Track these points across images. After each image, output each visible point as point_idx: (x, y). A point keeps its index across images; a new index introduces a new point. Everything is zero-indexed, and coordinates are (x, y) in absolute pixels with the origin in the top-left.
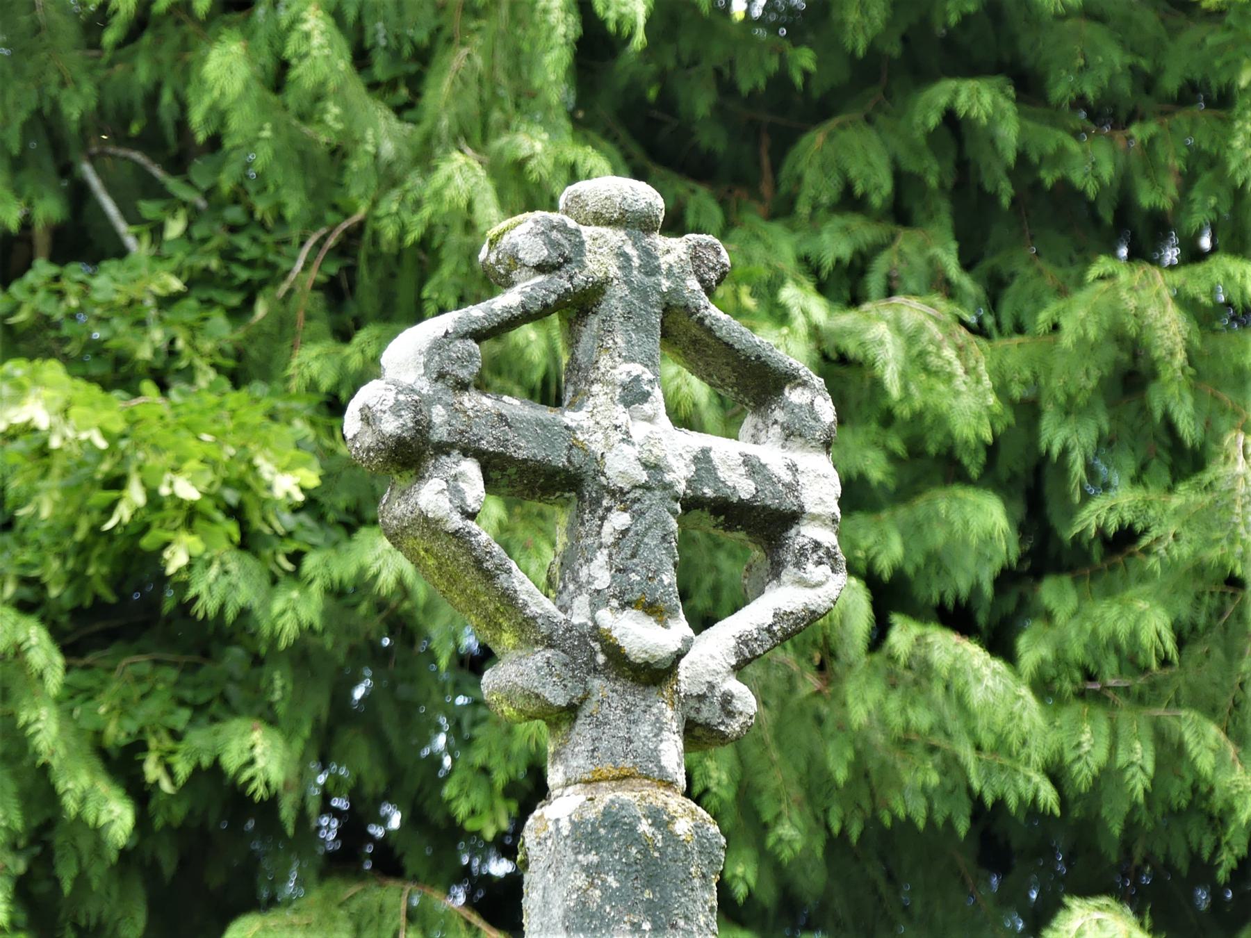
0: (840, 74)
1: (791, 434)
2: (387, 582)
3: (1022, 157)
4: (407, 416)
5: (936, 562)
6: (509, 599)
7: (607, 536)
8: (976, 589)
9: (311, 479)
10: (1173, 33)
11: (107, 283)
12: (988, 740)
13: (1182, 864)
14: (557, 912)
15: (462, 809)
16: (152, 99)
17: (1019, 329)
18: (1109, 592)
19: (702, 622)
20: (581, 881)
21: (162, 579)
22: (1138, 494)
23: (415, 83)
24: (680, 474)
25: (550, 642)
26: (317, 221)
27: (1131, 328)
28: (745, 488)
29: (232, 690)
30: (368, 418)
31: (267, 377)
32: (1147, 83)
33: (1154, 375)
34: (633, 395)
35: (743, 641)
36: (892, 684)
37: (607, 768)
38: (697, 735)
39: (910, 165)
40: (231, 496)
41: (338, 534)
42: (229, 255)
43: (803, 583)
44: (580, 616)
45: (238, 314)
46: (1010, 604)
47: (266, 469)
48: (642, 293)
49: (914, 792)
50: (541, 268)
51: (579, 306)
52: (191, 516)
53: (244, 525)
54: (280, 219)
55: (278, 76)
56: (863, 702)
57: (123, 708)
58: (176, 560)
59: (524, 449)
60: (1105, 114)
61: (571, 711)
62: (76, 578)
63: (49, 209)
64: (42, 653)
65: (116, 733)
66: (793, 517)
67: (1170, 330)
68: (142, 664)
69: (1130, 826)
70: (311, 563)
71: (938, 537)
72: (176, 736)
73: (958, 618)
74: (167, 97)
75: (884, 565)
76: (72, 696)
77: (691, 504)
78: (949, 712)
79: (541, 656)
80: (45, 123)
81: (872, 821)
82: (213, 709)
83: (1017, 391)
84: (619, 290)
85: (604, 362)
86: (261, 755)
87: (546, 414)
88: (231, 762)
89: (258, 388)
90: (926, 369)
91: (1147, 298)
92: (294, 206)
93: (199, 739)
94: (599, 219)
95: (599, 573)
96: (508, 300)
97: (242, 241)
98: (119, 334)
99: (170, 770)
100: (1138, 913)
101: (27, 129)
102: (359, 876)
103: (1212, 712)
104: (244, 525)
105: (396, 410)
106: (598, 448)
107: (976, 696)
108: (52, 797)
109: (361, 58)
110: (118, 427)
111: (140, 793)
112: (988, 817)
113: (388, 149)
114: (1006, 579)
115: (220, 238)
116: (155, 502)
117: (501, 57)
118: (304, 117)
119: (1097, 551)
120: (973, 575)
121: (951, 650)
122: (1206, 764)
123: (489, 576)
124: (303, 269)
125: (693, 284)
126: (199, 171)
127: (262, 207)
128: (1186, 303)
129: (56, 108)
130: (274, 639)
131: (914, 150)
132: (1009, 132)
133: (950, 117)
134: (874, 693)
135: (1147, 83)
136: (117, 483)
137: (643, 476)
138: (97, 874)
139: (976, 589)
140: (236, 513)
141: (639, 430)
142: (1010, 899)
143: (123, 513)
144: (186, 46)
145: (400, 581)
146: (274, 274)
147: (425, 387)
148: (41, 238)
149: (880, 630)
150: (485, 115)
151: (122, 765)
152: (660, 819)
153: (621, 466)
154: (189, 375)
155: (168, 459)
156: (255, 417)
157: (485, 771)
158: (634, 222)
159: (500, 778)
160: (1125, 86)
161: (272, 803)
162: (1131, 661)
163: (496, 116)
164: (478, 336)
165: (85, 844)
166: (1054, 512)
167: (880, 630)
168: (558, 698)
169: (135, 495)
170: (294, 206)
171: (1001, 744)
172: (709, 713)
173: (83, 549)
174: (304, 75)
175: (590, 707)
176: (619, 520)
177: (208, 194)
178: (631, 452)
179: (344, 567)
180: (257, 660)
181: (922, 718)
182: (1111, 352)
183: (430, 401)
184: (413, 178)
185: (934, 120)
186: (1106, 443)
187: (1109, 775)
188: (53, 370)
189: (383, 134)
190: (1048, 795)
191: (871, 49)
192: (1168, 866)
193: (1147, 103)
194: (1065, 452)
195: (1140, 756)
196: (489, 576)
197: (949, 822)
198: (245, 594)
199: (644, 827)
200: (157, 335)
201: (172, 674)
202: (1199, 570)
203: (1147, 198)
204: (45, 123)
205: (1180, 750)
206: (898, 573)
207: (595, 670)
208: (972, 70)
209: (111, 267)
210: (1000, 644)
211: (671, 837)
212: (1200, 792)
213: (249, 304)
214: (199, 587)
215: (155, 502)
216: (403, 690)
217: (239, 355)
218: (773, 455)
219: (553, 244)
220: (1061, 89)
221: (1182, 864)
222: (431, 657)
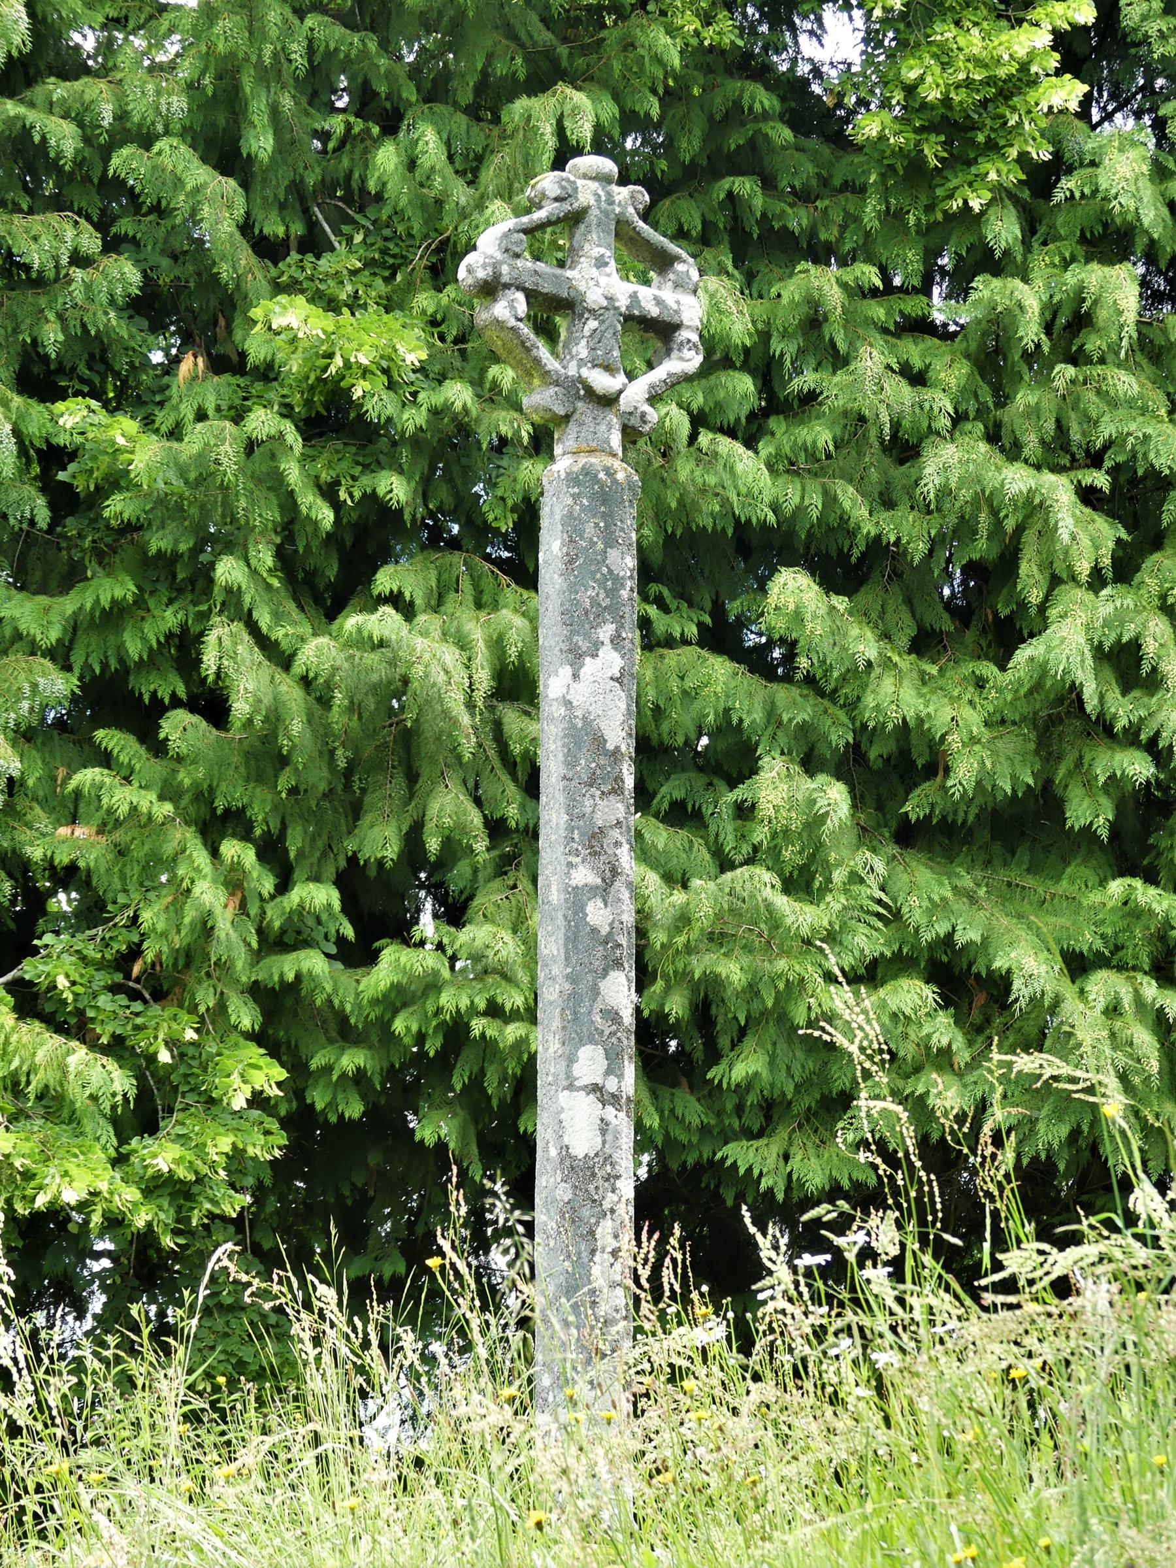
0: (679, 173)
1: (677, 286)
2: (458, 406)
3: (764, 215)
4: (490, 270)
5: (719, 406)
6: (537, 361)
7: (587, 332)
8: (738, 420)
9: (424, 356)
10: (838, 159)
11: (326, 263)
12: (744, 490)
13: (834, 554)
14: (558, 517)
15: (491, 517)
16: (349, 176)
17: (761, 297)
18: (802, 422)
19: (631, 376)
20: (570, 501)
21: (350, 401)
22: (818, 376)
23: (476, 171)
24: (623, 303)
25: (557, 383)
26: (426, 236)
27: (816, 295)
28: (654, 311)
29: (382, 458)
30: (470, 271)
31: (402, 309)
32: (825, 182)
33: (826, 319)
34: (600, 263)
35: (652, 386)
36: (698, 461)
37: (584, 446)
38: (630, 434)
39: (711, 217)
40: (384, 364)
41: (435, 384)
42: (384, 252)
43: (682, 359)
44: (572, 371)
45: (386, 280)
46: (754, 427)
47: (401, 350)
48: (606, 213)
49: (707, 514)
50: (556, 199)
51: (575, 218)
52: (365, 372)
53: (390, 378)
54: (411, 236)
55: (412, 164)
56: (685, 470)
57: (329, 465)
58: (357, 393)
59: (546, 288)
60: (803, 196)
61: (567, 418)
62: (308, 403)
63: (298, 229)
64: (293, 437)
65: (325, 477)
66: (677, 327)
67: (834, 297)
68: (339, 445)
69: (810, 534)
70: (421, 397)
71: (722, 394)
72: (354, 479)
73: (731, 432)
74: (356, 175)
75: (695, 407)
76: (304, 459)
77: (628, 318)
78: (726, 476)
79: (553, 390)
80: (297, 187)
81: (687, 528)
82: (371, 466)
83: (760, 326)
84: (594, 212)
85: (587, 247)
86: (396, 488)
87: (558, 271)
88: (381, 491)
89: (398, 313)
90: (720, 312)
91: (825, 283)
92: (417, 227)
93: (366, 481)
94: (584, 176)
95: (582, 350)
96: (540, 215)
97: (391, 245)
98: (330, 288)
99: (351, 495)
100: (813, 575)
101: (288, 190)
102: (440, 549)
103: (850, 481)
104: (390, 378)
105: (484, 266)
106: (582, 288)
107: (739, 468)
108: (294, 506)
109: (450, 158)
110: (331, 329)
111: (337, 506)
112: (742, 527)
113: (463, 201)
114: (752, 416)
115: (380, 244)
116: (347, 365)
117: (519, 157)
118: (422, 185)
119: (796, 403)
120: (738, 412)
121: (727, 445)
122: (847, 505)
123: (528, 350)
124: (419, 260)
125: (631, 210)
126: (371, 212)
127: (400, 229)
128: (844, 285)
129: (302, 180)
130: (403, 432)
131: (712, 210)
132: (758, 202)
133: (730, 194)
134: (692, 464)
135: (825, 182)
136: (330, 356)
137: (605, 303)
138: (315, 544)
139: (738, 420)
140: (386, 372)
141: (603, 280)
142: (751, 570)
143: (333, 369)
144: (366, 151)
145: (464, 406)
146: (406, 261)
147: (499, 256)
148: (293, 243)
149: (693, 438)
150: (511, 186)
151: (329, 492)
152: (609, 472)
153: (594, 298)
154: (365, 307)
155: (354, 345)
156: (397, 326)
157: (503, 499)
158: (603, 178)
159: (510, 503)
160: (814, 182)
161: (400, 511)
162: (812, 456)
163: (516, 185)
164: (526, 231)
165: (309, 529)
166: (777, 388)
167: (693, 438)
168: (561, 411)
169: (338, 361)
170: (417, 227)
171: (749, 494)
172: (634, 421)
173: (312, 388)
174: (425, 162)
175: (576, 416)
176: (593, 324)
177: (374, 222)
178: (599, 291)
179: (437, 399)
180: (394, 444)
181: (711, 480)
182: (805, 308)
183: (501, 263)
184: (476, 215)
185: (722, 196)
186: (801, 351)
187: (800, 510)
188: (300, 300)
189: (461, 194)
190: (771, 518)
191: (692, 160)
192: (828, 555)
193: (826, 191)
194: (782, 355)
195: (816, 500)
196: (528, 350)
197: (724, 530)
198: (390, 410)
199: (602, 475)
200: (349, 288)
201: (353, 449)
202: (845, 413)
203: (823, 236)
204: (297, 187)
205: (835, 499)
206: (701, 410)
207: (579, 398)
208: (739, 171)
209: (327, 256)
210: (750, 443)
211: (615, 481)
212: (844, 519)
213: (394, 275)
214: (368, 406)
215: (347, 365)
216: (464, 461)
217: (388, 299)
218: (669, 296)
219: (563, 188)
220: (783, 183)
221: (834, 554)
222: (479, 442)
